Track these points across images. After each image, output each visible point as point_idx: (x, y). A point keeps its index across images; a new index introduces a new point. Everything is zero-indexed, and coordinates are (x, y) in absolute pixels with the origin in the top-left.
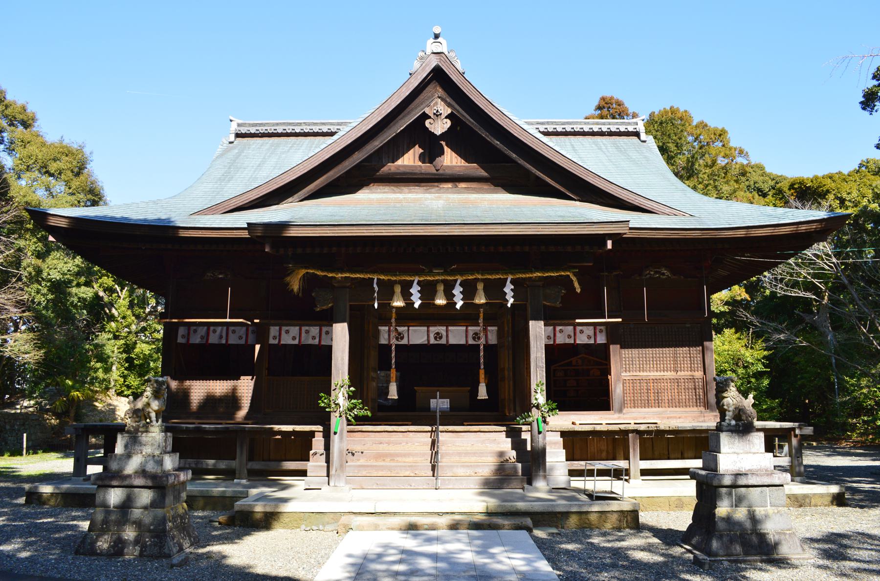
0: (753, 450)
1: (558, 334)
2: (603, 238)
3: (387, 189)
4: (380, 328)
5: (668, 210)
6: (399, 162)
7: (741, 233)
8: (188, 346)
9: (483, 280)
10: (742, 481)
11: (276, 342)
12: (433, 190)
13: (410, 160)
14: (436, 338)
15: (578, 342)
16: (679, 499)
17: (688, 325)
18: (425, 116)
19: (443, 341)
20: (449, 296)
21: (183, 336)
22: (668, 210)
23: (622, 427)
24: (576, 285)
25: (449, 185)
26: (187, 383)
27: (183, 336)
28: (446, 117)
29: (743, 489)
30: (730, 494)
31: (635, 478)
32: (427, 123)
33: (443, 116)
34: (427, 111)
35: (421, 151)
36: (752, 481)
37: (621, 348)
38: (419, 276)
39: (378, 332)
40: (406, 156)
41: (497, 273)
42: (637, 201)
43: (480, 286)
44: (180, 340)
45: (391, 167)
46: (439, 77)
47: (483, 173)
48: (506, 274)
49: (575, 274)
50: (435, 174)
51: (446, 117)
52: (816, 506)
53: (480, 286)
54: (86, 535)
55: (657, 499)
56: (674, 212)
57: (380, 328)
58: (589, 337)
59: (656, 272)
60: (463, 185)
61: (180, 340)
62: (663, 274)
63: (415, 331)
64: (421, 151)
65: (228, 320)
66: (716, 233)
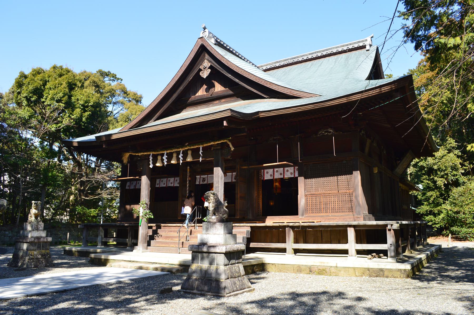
0: (218, 233)
1: (276, 173)
2: (222, 119)
3: (192, 109)
4: (357, 176)
5: (307, 95)
6: (197, 95)
7: (344, 100)
8: (129, 190)
9: (191, 149)
10: (212, 250)
11: (158, 186)
12: (210, 106)
13: (201, 93)
14: (203, 181)
15: (286, 177)
16: (299, 266)
17: (344, 162)
18: (200, 70)
19: (205, 183)
20: (178, 159)
21: (129, 186)
22: (307, 95)
23: (281, 224)
24: (231, 146)
25: (217, 102)
26: (132, 206)
27: (129, 186)
28: (209, 68)
29: (214, 254)
30: (208, 257)
31: (289, 254)
32: (201, 74)
33: (207, 68)
34: (201, 67)
35: (206, 87)
36: (217, 250)
37: (305, 178)
38: (167, 150)
39: (196, 178)
40: (200, 91)
41: (196, 145)
42: (295, 94)
43: (190, 152)
44: (127, 188)
45: (193, 98)
46: (202, 50)
47: (231, 92)
48: (199, 145)
49: (230, 141)
50: (210, 98)
51: (209, 68)
52: (387, 277)
53: (190, 152)
54: (211, 280)
55: (287, 266)
56: (310, 95)
57: (357, 176)
58: (291, 174)
59: (326, 132)
60: (223, 100)
61: (127, 188)
62: (330, 132)
63: (210, 177)
64: (206, 87)
65: (128, 178)
66: (322, 104)
